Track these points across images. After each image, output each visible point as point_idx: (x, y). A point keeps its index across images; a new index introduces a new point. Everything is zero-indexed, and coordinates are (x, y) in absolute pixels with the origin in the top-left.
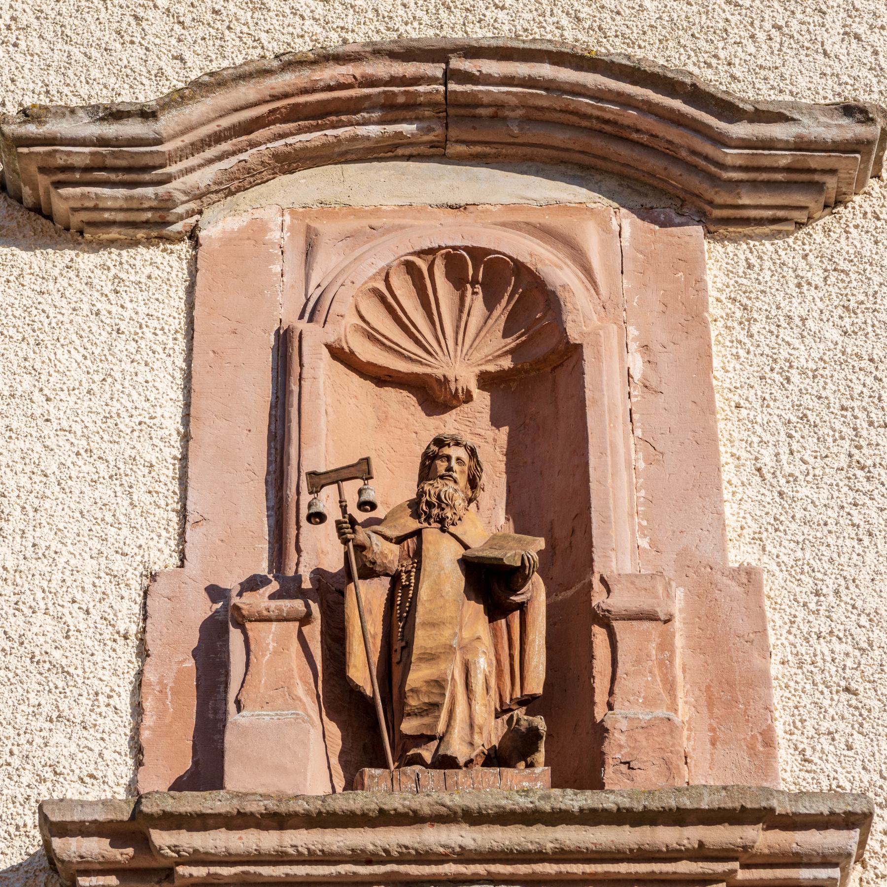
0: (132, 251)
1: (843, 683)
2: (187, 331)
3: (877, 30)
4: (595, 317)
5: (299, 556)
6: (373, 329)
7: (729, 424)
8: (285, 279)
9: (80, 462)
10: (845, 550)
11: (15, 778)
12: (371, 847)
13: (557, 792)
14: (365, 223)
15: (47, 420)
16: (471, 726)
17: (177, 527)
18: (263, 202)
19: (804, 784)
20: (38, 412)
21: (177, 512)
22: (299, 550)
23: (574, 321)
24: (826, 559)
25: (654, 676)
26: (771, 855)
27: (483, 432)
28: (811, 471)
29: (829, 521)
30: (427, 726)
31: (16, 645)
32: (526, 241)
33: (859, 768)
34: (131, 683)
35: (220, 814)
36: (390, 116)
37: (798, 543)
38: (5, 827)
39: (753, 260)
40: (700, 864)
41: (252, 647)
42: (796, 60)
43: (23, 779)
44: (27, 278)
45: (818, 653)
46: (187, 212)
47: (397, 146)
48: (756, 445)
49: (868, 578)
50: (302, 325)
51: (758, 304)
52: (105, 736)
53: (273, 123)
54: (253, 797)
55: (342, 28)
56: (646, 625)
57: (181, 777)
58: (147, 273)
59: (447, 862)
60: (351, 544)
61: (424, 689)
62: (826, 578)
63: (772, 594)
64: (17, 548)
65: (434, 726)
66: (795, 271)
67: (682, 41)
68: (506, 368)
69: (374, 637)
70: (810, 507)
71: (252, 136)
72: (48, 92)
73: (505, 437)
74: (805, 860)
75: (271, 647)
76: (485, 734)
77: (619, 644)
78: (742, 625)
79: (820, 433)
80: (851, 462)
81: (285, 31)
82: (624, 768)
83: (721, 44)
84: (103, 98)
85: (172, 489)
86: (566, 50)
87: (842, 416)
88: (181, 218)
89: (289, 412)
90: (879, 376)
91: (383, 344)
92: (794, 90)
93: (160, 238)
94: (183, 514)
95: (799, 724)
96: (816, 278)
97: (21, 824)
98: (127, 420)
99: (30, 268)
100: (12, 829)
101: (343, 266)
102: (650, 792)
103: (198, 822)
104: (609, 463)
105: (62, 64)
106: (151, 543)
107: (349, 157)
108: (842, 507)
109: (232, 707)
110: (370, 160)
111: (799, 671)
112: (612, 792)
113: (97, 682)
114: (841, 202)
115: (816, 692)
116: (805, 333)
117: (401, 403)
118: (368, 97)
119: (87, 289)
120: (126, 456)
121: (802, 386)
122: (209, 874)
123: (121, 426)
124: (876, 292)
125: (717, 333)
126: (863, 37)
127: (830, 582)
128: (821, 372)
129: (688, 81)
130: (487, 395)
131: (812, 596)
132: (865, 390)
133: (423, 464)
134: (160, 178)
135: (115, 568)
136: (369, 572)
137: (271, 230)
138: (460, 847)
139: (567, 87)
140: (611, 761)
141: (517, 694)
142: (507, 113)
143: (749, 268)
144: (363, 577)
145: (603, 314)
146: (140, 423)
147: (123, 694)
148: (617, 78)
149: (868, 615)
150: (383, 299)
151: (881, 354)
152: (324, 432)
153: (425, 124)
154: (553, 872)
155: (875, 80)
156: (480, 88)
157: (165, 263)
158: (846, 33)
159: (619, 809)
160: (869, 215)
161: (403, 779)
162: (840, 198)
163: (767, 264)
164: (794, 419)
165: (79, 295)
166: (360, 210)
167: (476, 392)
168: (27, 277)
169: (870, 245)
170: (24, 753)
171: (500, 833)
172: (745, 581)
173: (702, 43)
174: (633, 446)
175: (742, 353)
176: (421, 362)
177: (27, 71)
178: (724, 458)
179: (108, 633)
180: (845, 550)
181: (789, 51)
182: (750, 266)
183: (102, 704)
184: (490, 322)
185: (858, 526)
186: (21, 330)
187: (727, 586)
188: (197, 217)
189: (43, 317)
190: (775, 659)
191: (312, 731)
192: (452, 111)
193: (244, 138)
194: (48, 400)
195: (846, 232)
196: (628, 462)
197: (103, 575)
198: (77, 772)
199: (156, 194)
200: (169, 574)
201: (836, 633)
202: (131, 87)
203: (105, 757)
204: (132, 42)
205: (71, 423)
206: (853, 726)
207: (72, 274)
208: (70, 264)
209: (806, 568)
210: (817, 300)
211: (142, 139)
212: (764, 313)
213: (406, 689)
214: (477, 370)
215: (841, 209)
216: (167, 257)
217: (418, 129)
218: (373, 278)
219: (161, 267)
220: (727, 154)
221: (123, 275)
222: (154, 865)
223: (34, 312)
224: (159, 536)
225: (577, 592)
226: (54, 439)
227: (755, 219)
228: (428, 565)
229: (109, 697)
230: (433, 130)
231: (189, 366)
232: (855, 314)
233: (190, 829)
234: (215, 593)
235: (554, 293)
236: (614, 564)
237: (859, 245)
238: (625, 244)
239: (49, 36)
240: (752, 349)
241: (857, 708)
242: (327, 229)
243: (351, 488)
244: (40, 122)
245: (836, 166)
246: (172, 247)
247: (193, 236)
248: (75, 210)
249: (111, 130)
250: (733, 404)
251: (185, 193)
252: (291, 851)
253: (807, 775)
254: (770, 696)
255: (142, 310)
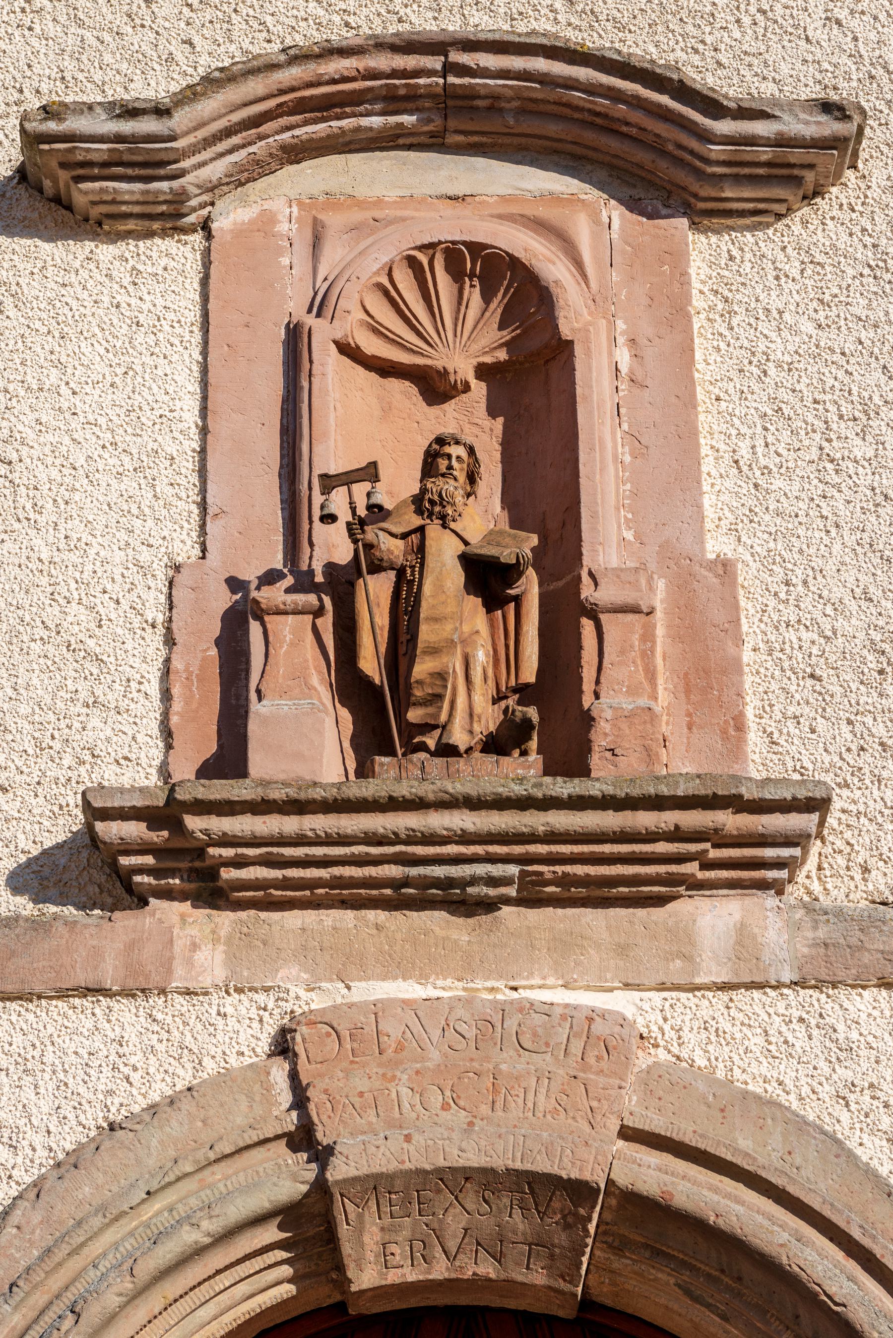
0: (149, 242)
1: (809, 670)
2: (202, 323)
3: (857, 15)
4: (585, 311)
5: (312, 550)
6: (377, 322)
7: (710, 416)
8: (293, 271)
9: (106, 455)
10: (814, 541)
11: (57, 760)
12: (381, 831)
13: (548, 780)
14: (369, 215)
15: (74, 414)
16: (471, 715)
17: (197, 519)
18: (271, 192)
19: (771, 765)
20: (65, 405)
21: (198, 504)
22: (311, 544)
23: (566, 317)
24: (796, 549)
25: (636, 666)
26: (740, 836)
27: (480, 422)
28: (784, 464)
29: (800, 513)
30: (431, 715)
31: (53, 634)
32: (521, 235)
33: (821, 750)
34: (159, 670)
35: (246, 802)
36: (391, 108)
37: (771, 534)
38: (49, 807)
39: (735, 252)
40: (676, 845)
41: (271, 639)
42: (779, 46)
43: (64, 762)
44: (49, 273)
45: (787, 640)
46: (200, 204)
47: (398, 136)
48: (734, 437)
49: (834, 568)
50: (310, 321)
51: (739, 297)
52: (138, 720)
53: (281, 115)
54: (275, 786)
55: (345, 11)
56: (630, 617)
57: (208, 760)
58: (163, 264)
59: (449, 843)
60: (360, 543)
61: (428, 680)
62: (795, 568)
63: (746, 584)
64: (51, 540)
65: (437, 715)
66: (774, 263)
67: (671, 25)
68: (502, 359)
69: (382, 629)
70: (783, 499)
71: (261, 129)
72: (63, 78)
73: (501, 427)
74: (769, 840)
75: (288, 639)
76: (483, 722)
77: (605, 636)
78: (718, 615)
79: (794, 426)
80: (821, 455)
81: (289, 14)
82: (608, 754)
83: (708, 29)
84: (119, 94)
85: (192, 481)
86: (560, 45)
87: (815, 409)
88: (194, 210)
89: (300, 408)
90: (850, 370)
91: (387, 337)
92: (777, 77)
93: (175, 229)
94: (203, 506)
95: (768, 709)
96: (793, 271)
97: (64, 804)
98: (149, 413)
99: (53, 259)
100: (56, 809)
101: (348, 259)
102: (631, 780)
103: (227, 808)
104: (598, 459)
105: (76, 48)
106: (174, 535)
107: (352, 147)
108: (812, 499)
109: (253, 696)
110: (372, 150)
111: (769, 658)
112: (598, 779)
113: (128, 669)
114: (818, 193)
115: (784, 678)
116: (782, 327)
117: (404, 393)
118: (370, 89)
119: (107, 280)
120: (149, 449)
121: (778, 379)
122: (236, 855)
123: (143, 419)
124: (849, 286)
125: (699, 325)
126: (844, 22)
127: (799, 572)
128: (796, 365)
129: (675, 77)
130: (483, 385)
131: (782, 586)
132: (836, 384)
133: (425, 462)
134: (174, 173)
135: (141, 559)
136: (376, 568)
137: (280, 222)
138: (462, 830)
139: (561, 81)
140: (596, 748)
141: (513, 683)
142: (503, 104)
143: (730, 260)
144: (371, 572)
145: (593, 307)
146: (161, 416)
147: (152, 680)
148: (608, 73)
149: (833, 604)
150: (386, 293)
151: (852, 348)
152: (333, 428)
153: (425, 115)
154: (544, 852)
155: (854, 67)
156: (478, 81)
157: (180, 254)
158: (827, 18)
159: (604, 796)
160: (845, 207)
161: (410, 767)
162: (818, 189)
163: (748, 256)
164: (770, 412)
165: (99, 287)
166: (364, 202)
167: (473, 382)
168: (51, 269)
169: (845, 237)
170: (65, 737)
171: (497, 818)
172: (722, 573)
173: (690, 28)
174: (620, 440)
175: (723, 346)
176: (422, 354)
177: (42, 56)
178: (704, 450)
179: (137, 622)
180: (814, 541)
181: (772, 36)
182: (732, 258)
183: (134, 690)
184: (487, 314)
185: (827, 518)
186: (46, 323)
187: (705, 577)
188: (209, 208)
189: (66, 310)
190: (748, 646)
191: (327, 720)
192: (450, 103)
193: (253, 131)
194: (74, 393)
195: (823, 224)
196: (615, 456)
197: (130, 566)
198: (113, 754)
199: (171, 188)
200: (191, 565)
201: (804, 621)
202: (143, 73)
203: (138, 740)
204: (143, 26)
205: (97, 416)
206: (816, 710)
207: (92, 266)
208: (90, 256)
209: (778, 559)
210: (794, 292)
211: (157, 136)
212: (744, 306)
213: (413, 680)
214: (475, 362)
215: (818, 200)
216: (181, 247)
217: (417, 120)
218: (377, 273)
219: (176, 258)
220: (711, 150)
221: (140, 267)
222: (187, 845)
223: (58, 305)
224: (182, 528)
225: (568, 583)
226: (81, 433)
227: (737, 211)
228: (431, 561)
229: (140, 683)
230: (433, 121)
231: (205, 359)
232: (829, 307)
233: (219, 815)
234: (234, 584)
235: (547, 288)
236: (601, 558)
237: (834, 237)
238: (615, 236)
239: (63, 19)
240: (732, 341)
241: (820, 693)
242: (333, 220)
243: (360, 490)
244: (60, 119)
245: (814, 161)
246: (186, 237)
247: (206, 226)
248: (94, 203)
249: (127, 127)
250: (713, 397)
251: (198, 186)
252: (310, 834)
253: (774, 757)
254: (742, 683)
255: (160, 302)
